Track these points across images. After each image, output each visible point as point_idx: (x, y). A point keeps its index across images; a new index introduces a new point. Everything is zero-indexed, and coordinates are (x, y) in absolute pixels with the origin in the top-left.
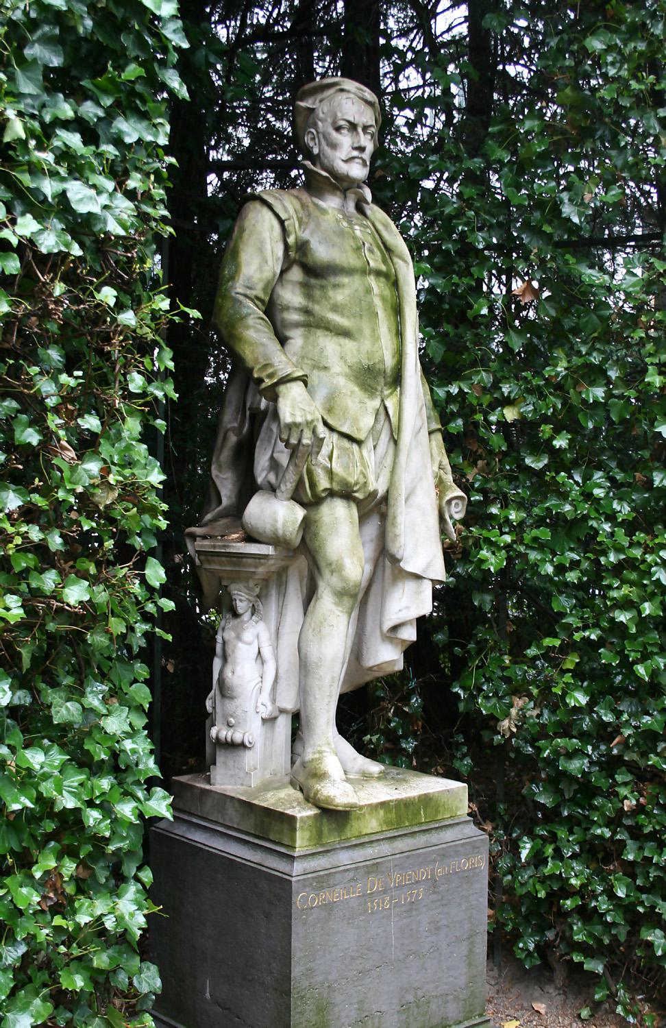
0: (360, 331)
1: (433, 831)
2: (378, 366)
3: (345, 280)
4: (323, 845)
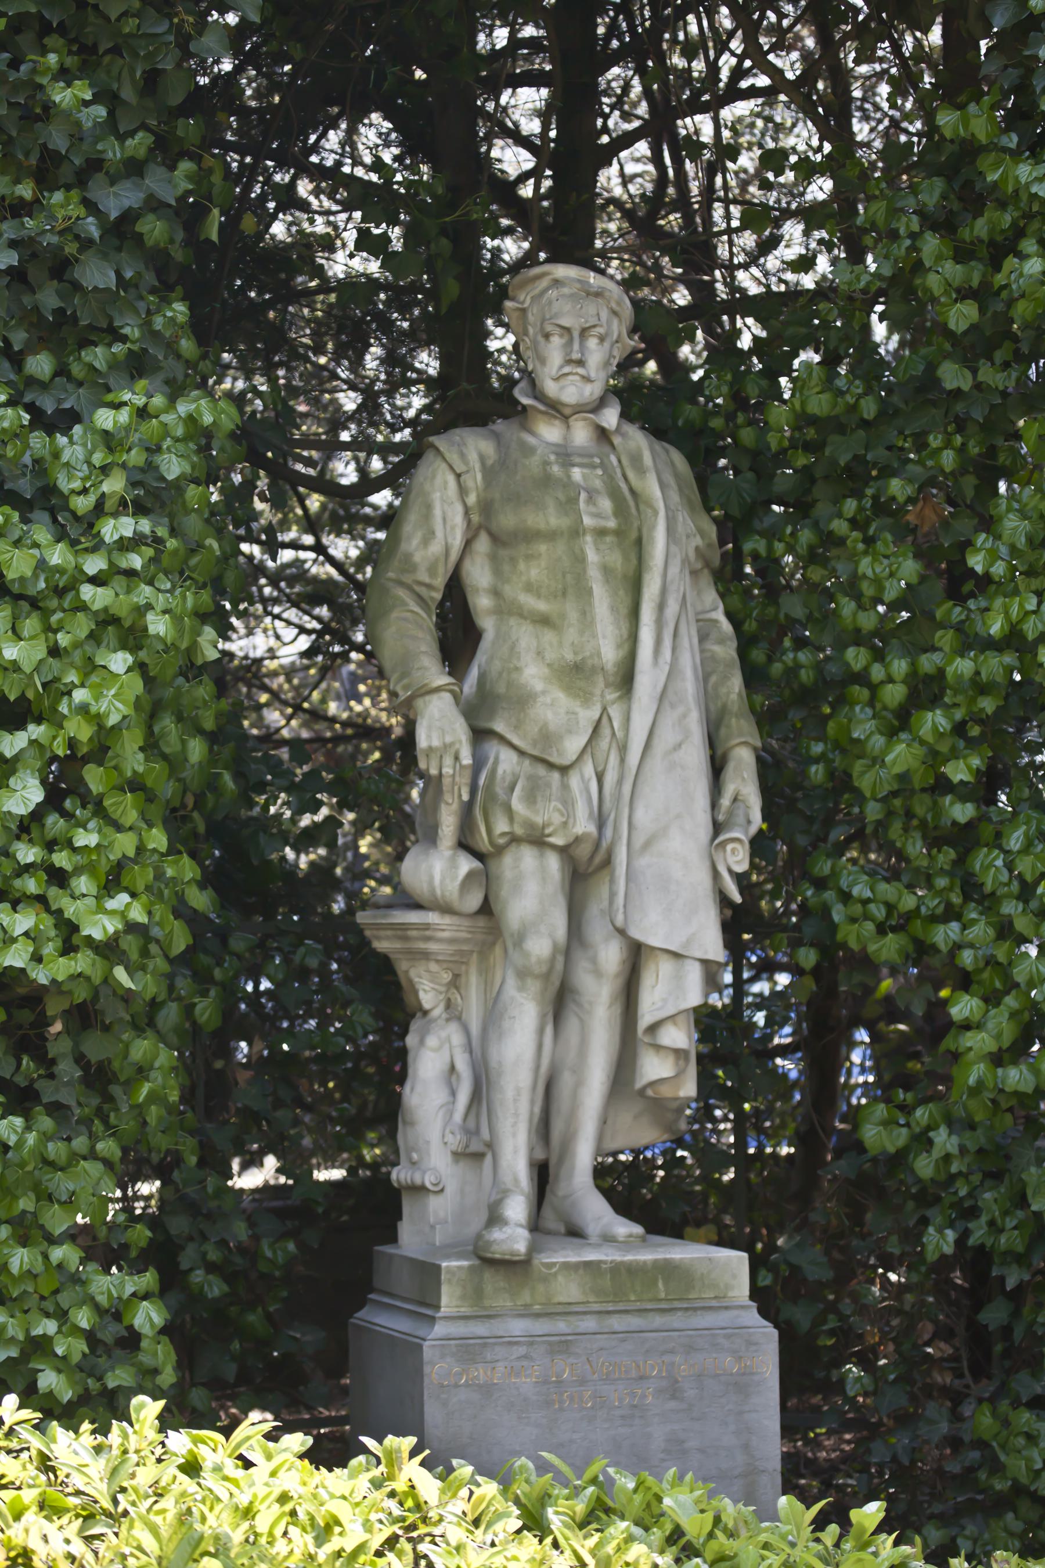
0: (563, 616)
1: (679, 1314)
2: (590, 662)
3: (543, 548)
4: (485, 1308)
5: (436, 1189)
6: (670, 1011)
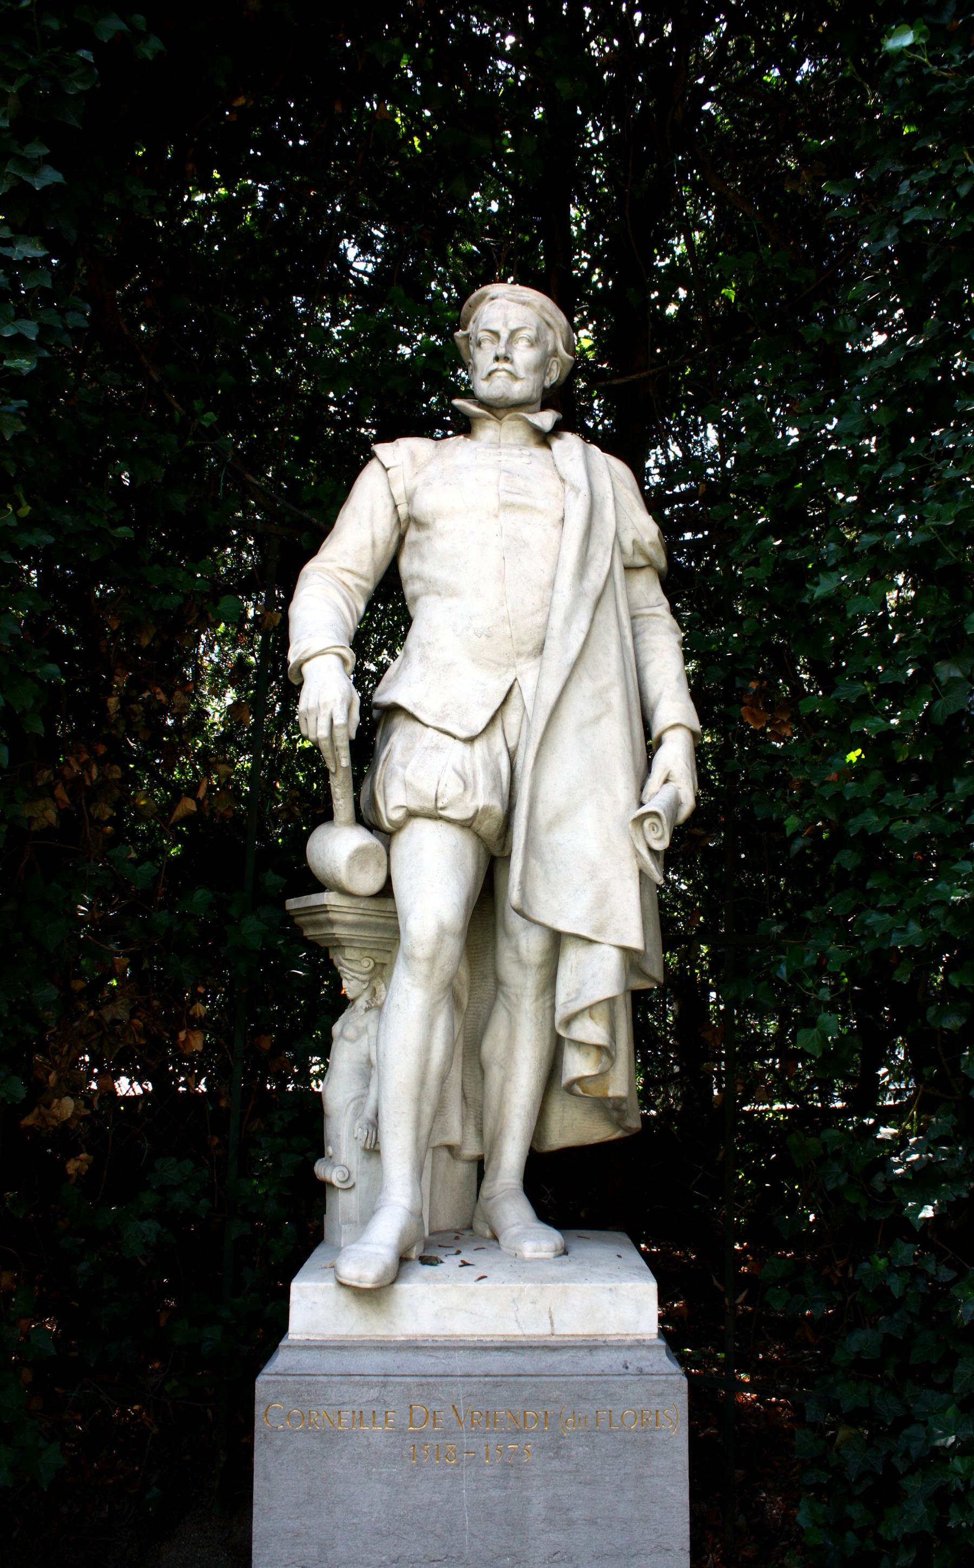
5: (344, 1186)
6: (584, 1002)
